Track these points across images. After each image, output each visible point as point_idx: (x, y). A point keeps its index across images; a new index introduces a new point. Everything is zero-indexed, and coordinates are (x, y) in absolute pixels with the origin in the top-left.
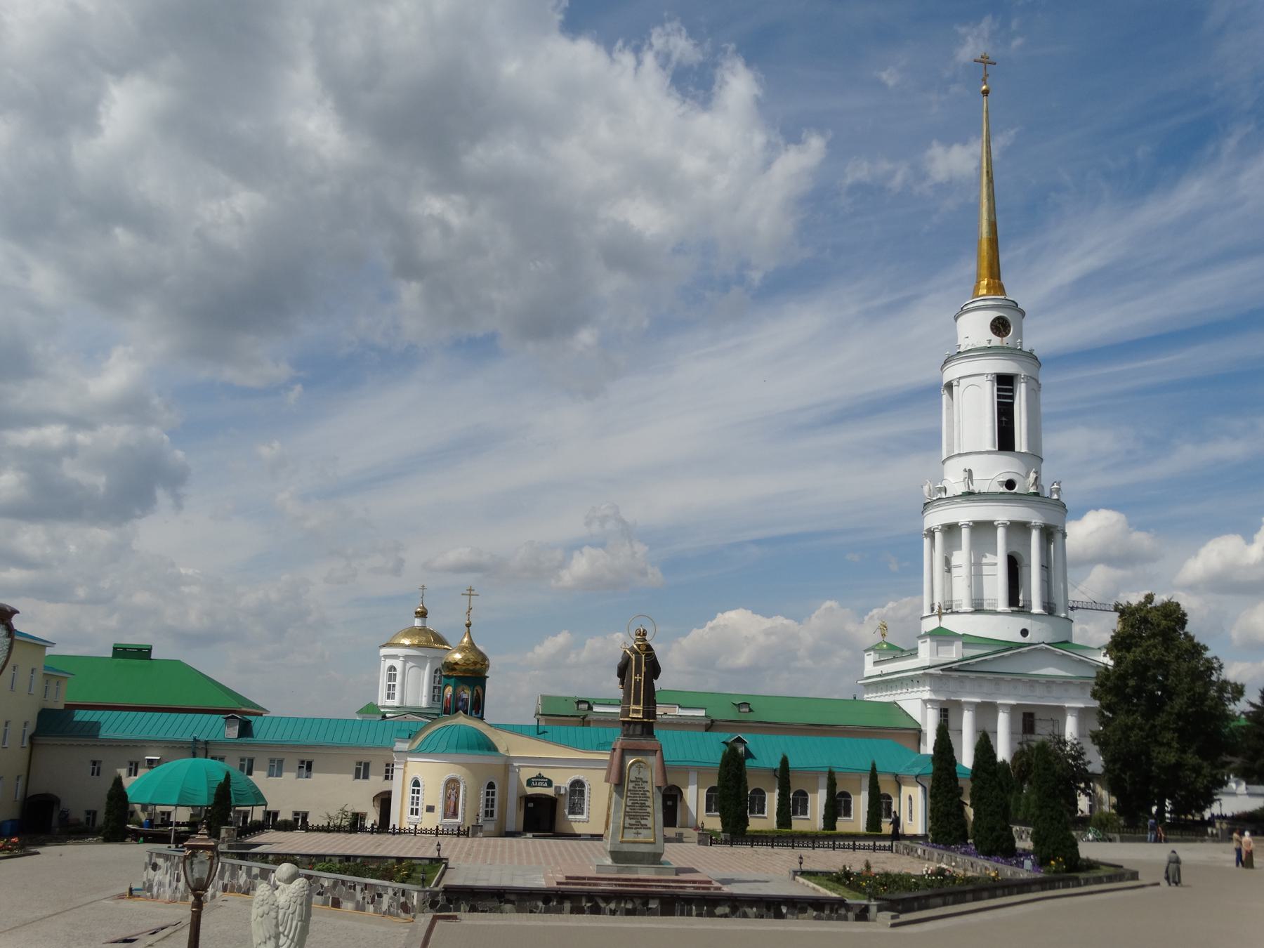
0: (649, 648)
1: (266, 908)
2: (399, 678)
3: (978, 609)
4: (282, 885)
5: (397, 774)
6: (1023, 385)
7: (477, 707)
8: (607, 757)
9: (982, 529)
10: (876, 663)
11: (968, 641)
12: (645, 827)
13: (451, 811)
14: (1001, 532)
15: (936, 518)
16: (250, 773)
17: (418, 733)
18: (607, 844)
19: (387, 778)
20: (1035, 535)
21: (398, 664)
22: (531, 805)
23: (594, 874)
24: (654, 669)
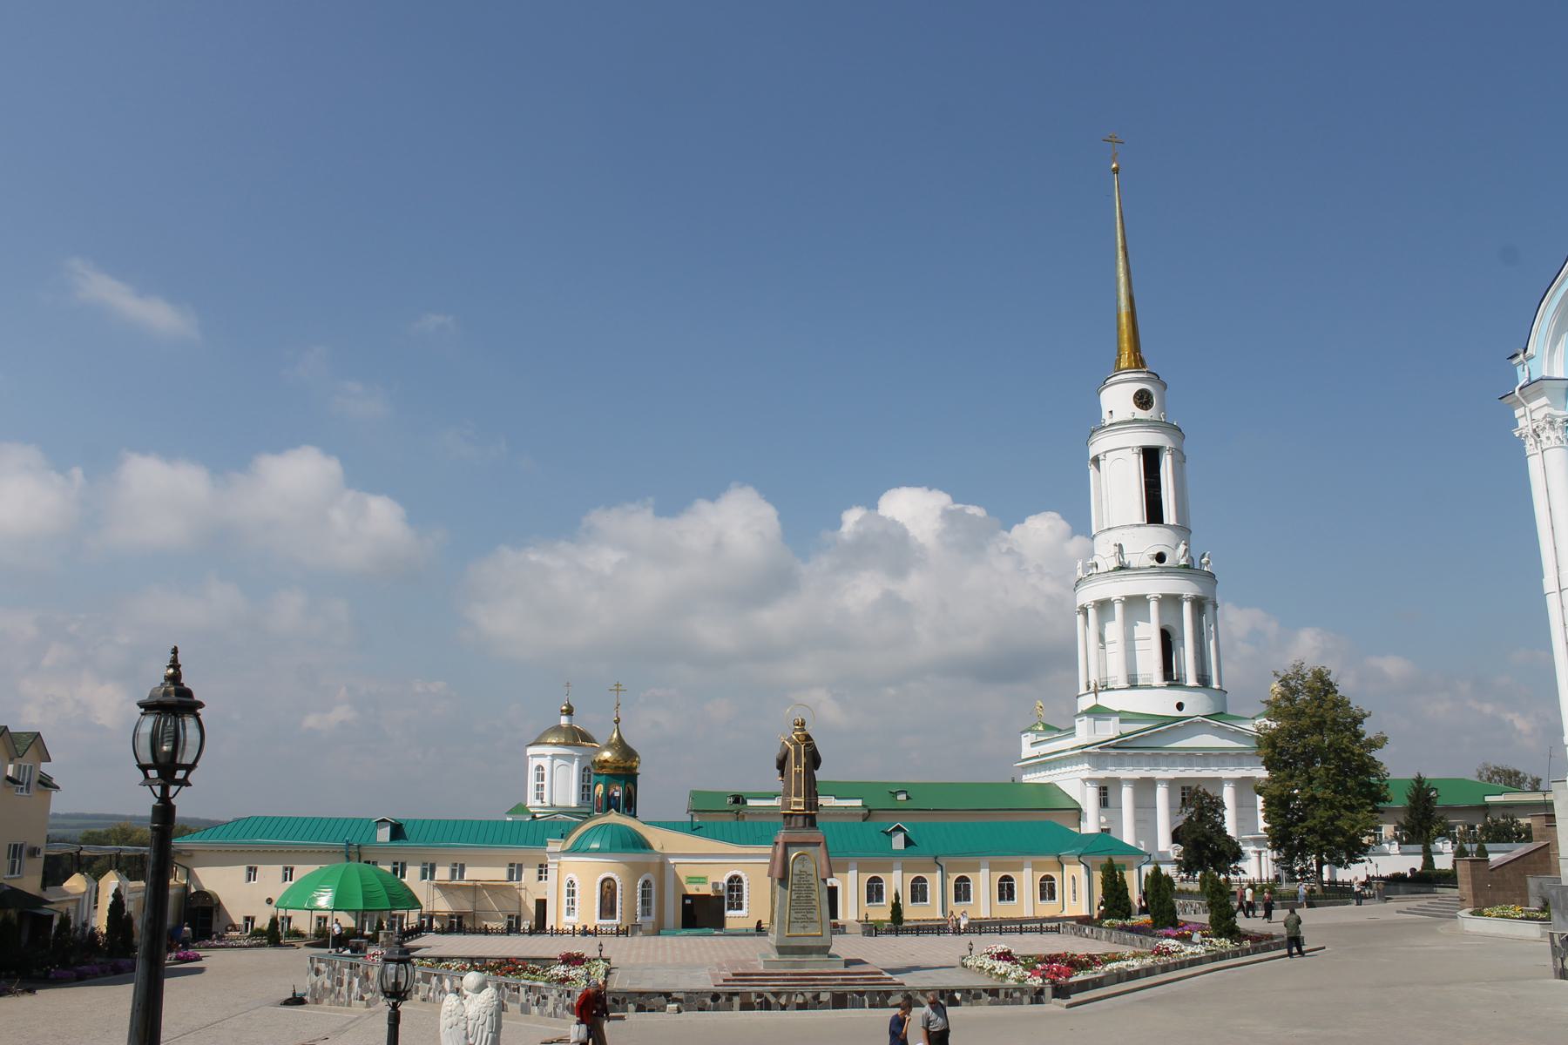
0: (808, 738)
1: (454, 1019)
2: (547, 777)
3: (1133, 685)
4: (471, 995)
5: (552, 874)
6: (1169, 458)
7: (629, 805)
8: (770, 851)
9: (1135, 604)
10: (1033, 744)
11: (1126, 717)
12: (812, 921)
13: (607, 909)
14: (1153, 606)
15: (1088, 595)
16: (403, 875)
17: (570, 833)
18: (772, 939)
20: (1187, 607)
21: (546, 763)
23: (761, 969)
24: (814, 760)
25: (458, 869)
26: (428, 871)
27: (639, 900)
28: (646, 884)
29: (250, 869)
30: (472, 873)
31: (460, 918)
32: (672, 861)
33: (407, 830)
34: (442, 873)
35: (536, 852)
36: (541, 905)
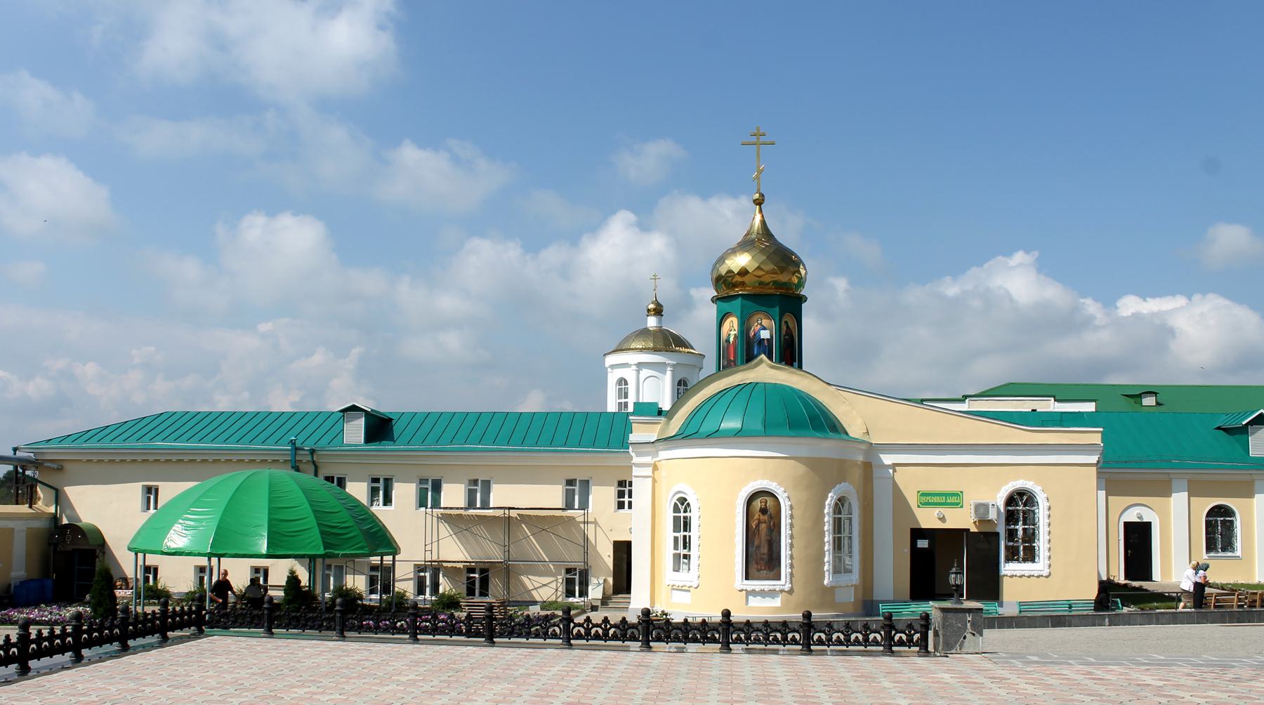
5: (641, 491)
7: (790, 353)
13: (762, 556)
19: (621, 506)
22: (923, 544)
25: (479, 489)
26: (430, 492)
27: (828, 538)
28: (840, 504)
29: (149, 490)
30: (504, 495)
31: (484, 571)
32: (888, 459)
33: (397, 429)
34: (454, 495)
35: (612, 459)
36: (623, 551)
